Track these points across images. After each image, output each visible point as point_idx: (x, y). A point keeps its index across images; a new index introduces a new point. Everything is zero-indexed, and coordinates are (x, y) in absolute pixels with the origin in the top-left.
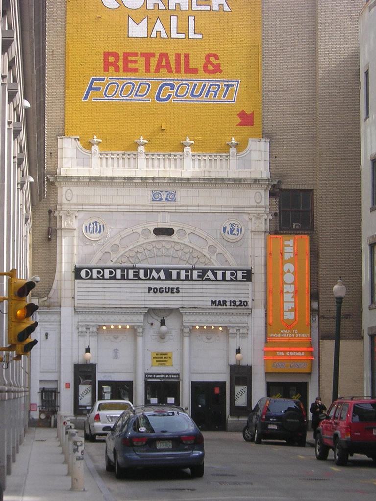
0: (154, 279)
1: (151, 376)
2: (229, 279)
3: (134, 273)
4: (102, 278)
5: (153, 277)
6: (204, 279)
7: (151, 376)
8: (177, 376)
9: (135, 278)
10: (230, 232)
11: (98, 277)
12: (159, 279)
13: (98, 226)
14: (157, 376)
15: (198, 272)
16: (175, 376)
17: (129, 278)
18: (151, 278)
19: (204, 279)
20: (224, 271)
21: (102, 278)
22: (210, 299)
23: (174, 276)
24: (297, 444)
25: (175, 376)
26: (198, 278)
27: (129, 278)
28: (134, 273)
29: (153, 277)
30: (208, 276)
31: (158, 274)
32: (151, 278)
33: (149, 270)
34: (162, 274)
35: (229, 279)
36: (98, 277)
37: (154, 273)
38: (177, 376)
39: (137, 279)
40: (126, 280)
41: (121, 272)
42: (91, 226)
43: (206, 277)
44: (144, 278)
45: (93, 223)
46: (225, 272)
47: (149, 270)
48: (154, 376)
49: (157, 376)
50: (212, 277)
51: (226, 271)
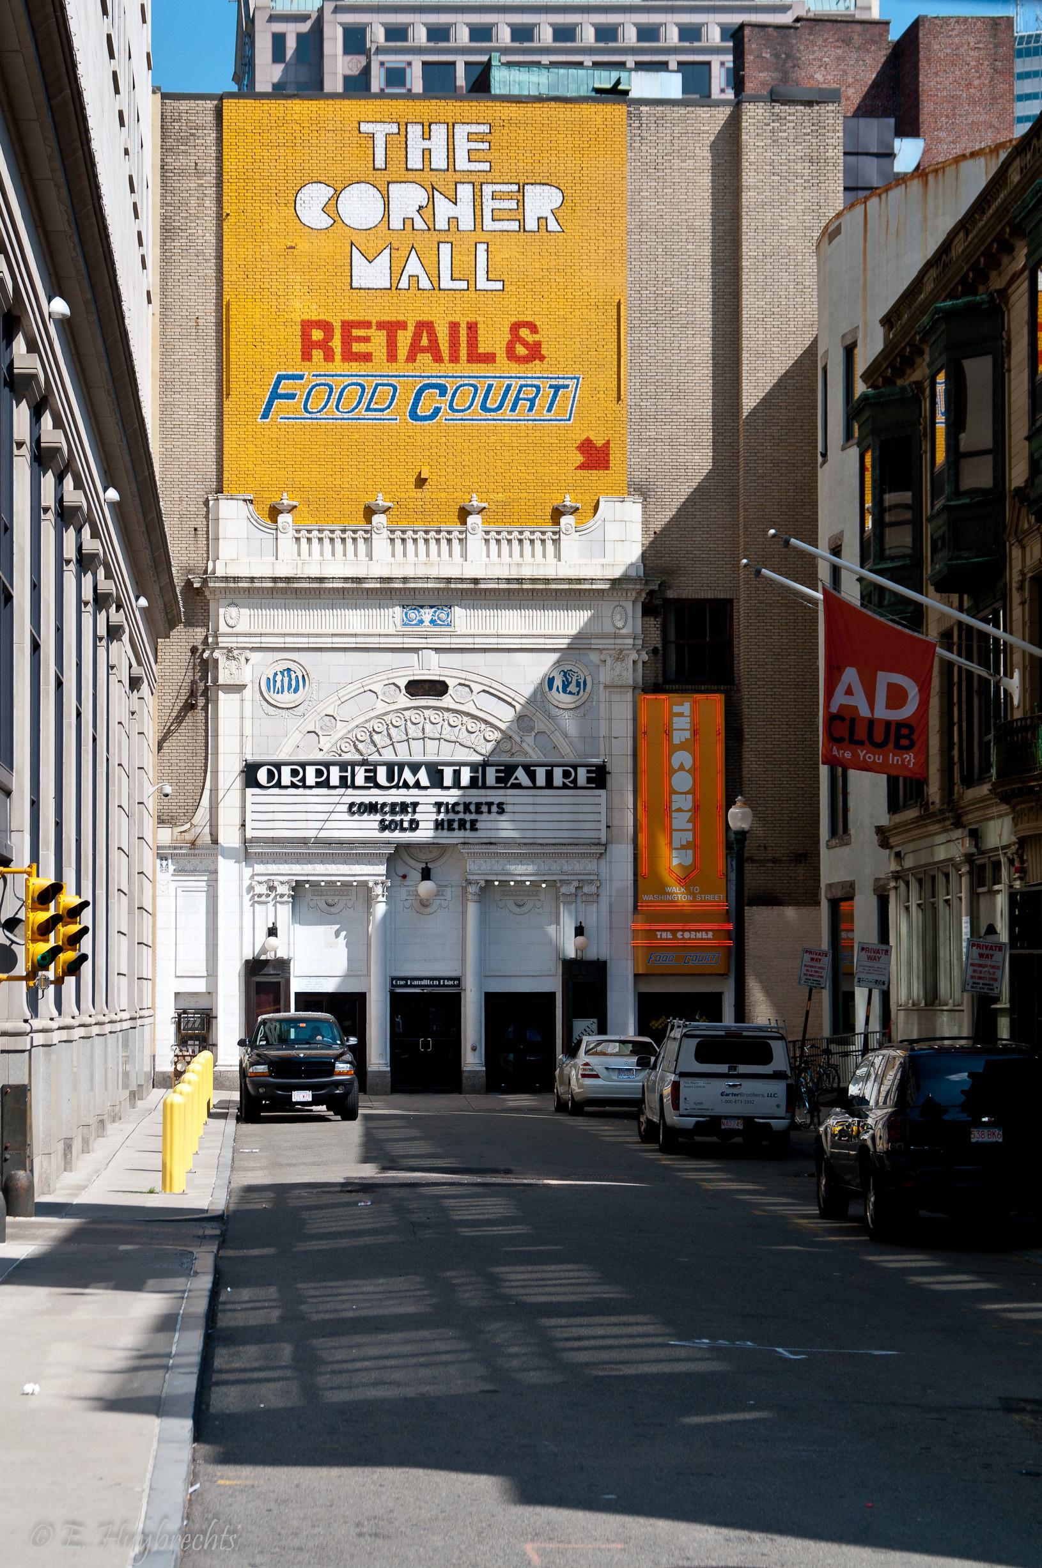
0: (406, 785)
12: (417, 785)
13: (293, 676)
14: (416, 983)
16: (451, 983)
25: (451, 983)
34: (423, 777)
35: (561, 785)
37: (407, 775)
43: (512, 781)
46: (459, 771)
49: (416, 983)
50: (524, 779)
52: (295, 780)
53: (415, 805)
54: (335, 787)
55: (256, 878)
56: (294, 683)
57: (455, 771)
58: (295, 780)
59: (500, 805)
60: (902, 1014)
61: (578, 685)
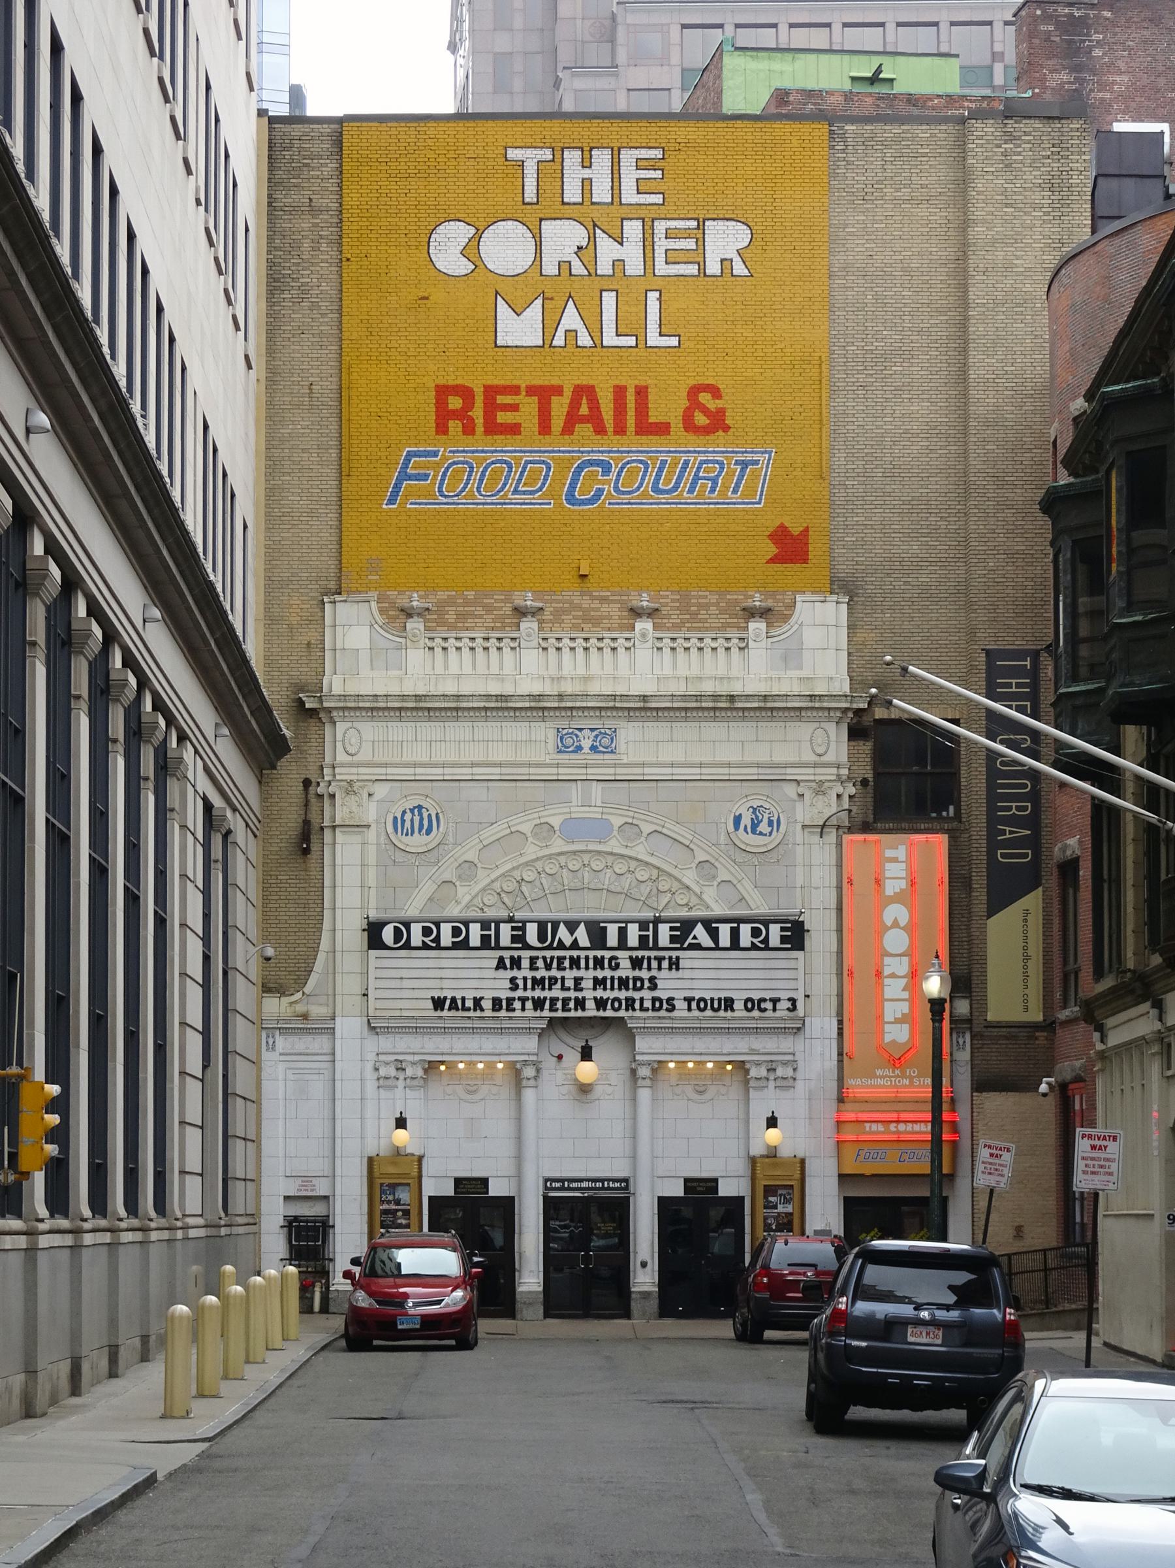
1: (558, 1185)
6: (686, 945)
7: (558, 1185)
13: (425, 815)
14: (575, 1185)
16: (617, 1185)
19: (686, 945)
25: (617, 1185)
37: (563, 933)
42: (408, 816)
43: (690, 940)
46: (625, 928)
49: (575, 1185)
50: (706, 940)
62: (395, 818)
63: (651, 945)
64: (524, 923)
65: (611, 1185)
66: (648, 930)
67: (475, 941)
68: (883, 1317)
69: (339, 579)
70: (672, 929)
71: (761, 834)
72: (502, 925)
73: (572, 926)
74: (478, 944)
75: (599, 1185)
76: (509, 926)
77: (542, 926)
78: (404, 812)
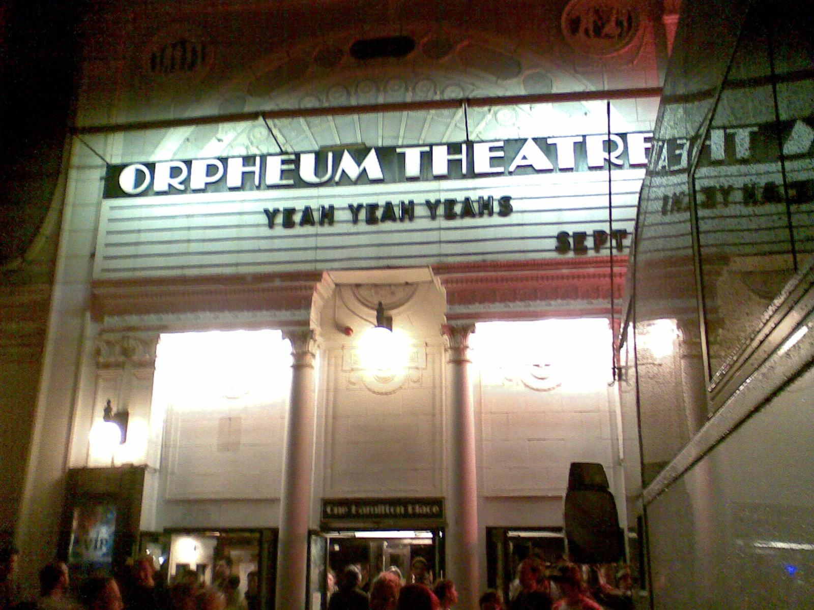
0: (345, 179)
1: (342, 510)
2: (166, 188)
3: (285, 167)
4: (182, 187)
5: (343, 171)
6: (512, 168)
7: (342, 510)
8: (435, 509)
9: (285, 182)
10: (594, 30)
11: (170, 185)
12: (363, 178)
13: (189, 49)
14: (366, 510)
15: (491, 149)
16: (426, 510)
17: (477, 170)
18: (337, 178)
19: (512, 168)
20: (427, 149)
21: (182, 187)
22: (555, 231)
23: (413, 165)
24: (423, 547)
25: (426, 510)
26: (491, 166)
27: (477, 170)
28: (285, 167)
29: (343, 171)
30: (524, 158)
31: (359, 165)
32: (337, 178)
33: (330, 155)
34: (372, 163)
35: (166, 188)
36: (170, 185)
37: (348, 164)
38: (435, 509)
39: (291, 182)
40: (464, 177)
41: (449, 153)
42: (169, 51)
43: (518, 161)
44: (315, 180)
45: (174, 46)
46: (430, 153)
47: (330, 155)
48: (354, 509)
49: (366, 510)
50: (538, 158)
51: (434, 148)
52: (175, 182)
53: (664, 212)
54: (719, 163)
55: (106, 336)
56: (189, 55)
57: (422, 154)
58: (175, 182)
59: (505, 202)
60: (44, 239)
61: (619, 23)
62: (154, 55)
63: (464, 171)
64: (298, 155)
65: (418, 510)
66: (460, 152)
67: (234, 179)
68: (214, 441)
69: (682, 235)
70: (491, 149)
71: (608, 36)
72: (269, 159)
73: (359, 154)
74: (238, 183)
75: (400, 510)
76: (279, 159)
77: (320, 157)
78: (163, 50)
